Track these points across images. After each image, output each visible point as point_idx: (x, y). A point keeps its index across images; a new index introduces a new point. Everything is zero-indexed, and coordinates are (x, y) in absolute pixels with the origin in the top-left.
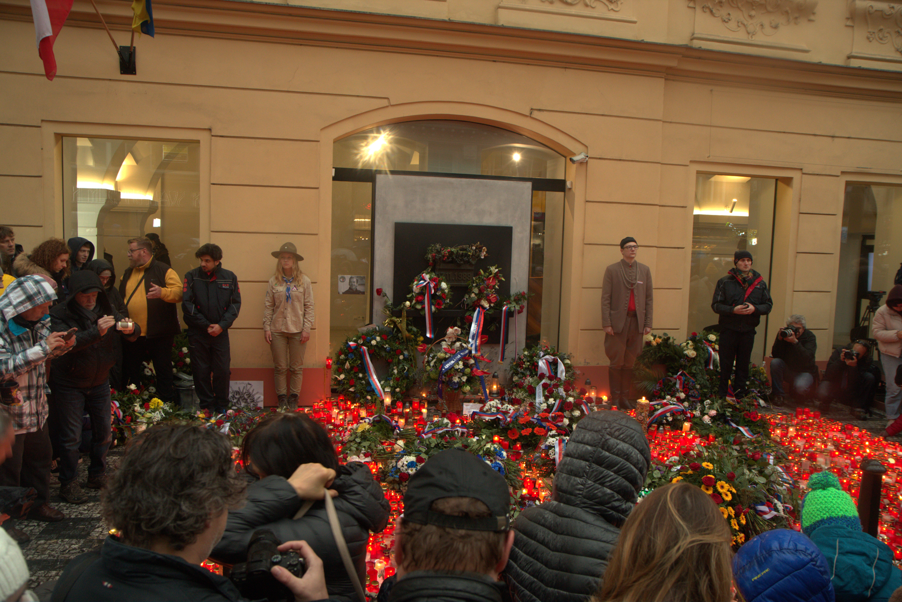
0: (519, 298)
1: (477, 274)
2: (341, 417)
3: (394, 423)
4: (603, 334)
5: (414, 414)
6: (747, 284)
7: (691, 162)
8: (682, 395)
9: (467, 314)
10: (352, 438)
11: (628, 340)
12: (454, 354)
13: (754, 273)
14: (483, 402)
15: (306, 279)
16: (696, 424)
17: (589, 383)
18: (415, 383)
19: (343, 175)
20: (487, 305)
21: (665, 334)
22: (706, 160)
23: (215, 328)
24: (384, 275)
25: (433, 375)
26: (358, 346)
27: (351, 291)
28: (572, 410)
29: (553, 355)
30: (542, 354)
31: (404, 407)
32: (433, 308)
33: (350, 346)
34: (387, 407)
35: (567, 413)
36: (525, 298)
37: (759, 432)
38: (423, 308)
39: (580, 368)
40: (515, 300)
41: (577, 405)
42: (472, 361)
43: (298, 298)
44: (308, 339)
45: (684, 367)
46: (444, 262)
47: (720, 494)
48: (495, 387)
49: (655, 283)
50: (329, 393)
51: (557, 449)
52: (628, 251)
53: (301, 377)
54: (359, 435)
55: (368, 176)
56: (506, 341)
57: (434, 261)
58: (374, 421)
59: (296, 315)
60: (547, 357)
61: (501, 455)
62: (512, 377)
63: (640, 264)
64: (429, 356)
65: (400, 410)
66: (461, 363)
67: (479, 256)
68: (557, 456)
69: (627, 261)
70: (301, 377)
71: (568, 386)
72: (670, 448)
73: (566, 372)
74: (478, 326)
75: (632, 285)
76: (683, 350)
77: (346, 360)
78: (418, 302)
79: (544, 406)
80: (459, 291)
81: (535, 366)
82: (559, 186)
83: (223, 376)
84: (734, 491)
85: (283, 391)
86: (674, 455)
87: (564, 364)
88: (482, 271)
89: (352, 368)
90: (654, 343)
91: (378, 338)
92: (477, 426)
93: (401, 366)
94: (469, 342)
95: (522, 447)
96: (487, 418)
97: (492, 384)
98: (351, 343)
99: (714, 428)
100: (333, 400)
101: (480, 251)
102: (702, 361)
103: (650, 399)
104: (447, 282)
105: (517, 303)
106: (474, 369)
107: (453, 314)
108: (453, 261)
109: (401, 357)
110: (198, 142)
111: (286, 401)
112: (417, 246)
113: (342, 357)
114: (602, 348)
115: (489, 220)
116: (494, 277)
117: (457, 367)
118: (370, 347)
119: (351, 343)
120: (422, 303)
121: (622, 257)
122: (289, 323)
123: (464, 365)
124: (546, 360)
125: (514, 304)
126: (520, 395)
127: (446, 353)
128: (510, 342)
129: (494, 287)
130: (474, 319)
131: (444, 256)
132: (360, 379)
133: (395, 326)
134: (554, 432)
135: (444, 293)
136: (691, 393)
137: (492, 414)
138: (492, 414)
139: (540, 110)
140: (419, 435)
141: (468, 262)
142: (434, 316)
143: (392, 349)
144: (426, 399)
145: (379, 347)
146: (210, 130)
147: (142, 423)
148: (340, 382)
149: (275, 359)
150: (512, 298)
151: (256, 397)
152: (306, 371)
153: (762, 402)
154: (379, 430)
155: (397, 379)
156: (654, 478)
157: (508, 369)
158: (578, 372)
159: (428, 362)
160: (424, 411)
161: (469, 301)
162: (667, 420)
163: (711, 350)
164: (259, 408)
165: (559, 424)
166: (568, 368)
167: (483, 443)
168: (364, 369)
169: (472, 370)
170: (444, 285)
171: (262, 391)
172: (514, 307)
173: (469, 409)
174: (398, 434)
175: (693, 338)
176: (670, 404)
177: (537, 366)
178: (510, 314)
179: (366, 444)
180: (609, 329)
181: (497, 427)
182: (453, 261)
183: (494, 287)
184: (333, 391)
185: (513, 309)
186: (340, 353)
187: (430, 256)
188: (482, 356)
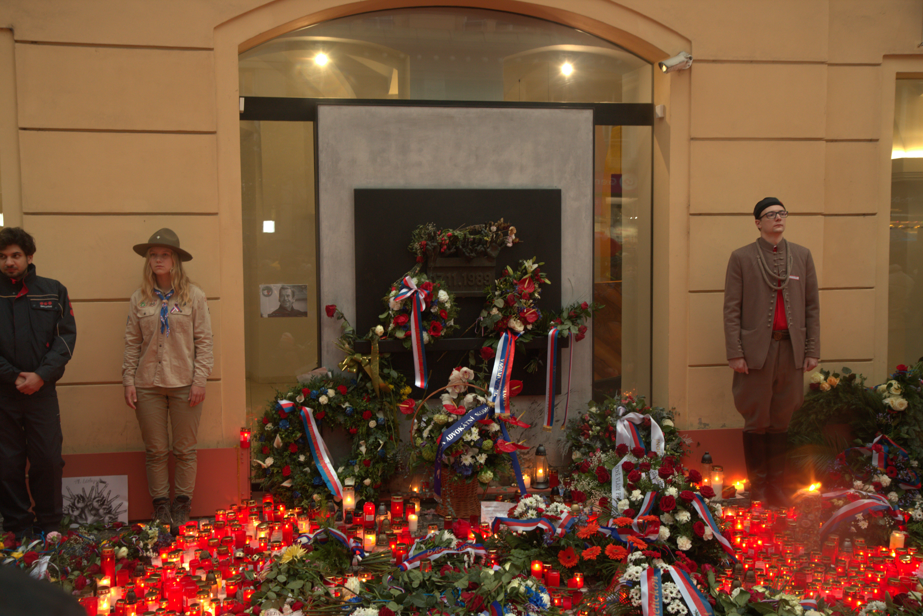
0: (577, 314)
1: (502, 274)
2: (262, 534)
3: (352, 543)
4: (728, 374)
5: (392, 524)
7: (886, 57)
9: (486, 344)
10: (272, 575)
11: (775, 383)
12: (464, 415)
14: (516, 499)
15: (197, 293)
16: (915, 534)
17: (709, 461)
18: (397, 468)
19: (257, 109)
20: (519, 328)
21: (846, 370)
23: (29, 380)
24: (340, 284)
25: (427, 454)
26: (296, 408)
27: (283, 312)
28: (676, 512)
29: (642, 411)
30: (621, 410)
31: (377, 512)
32: (426, 336)
33: (281, 407)
34: (348, 513)
35: (666, 517)
36: (587, 314)
38: (408, 336)
39: (691, 434)
41: (684, 502)
42: (495, 427)
43: (181, 325)
44: (202, 397)
45: (885, 429)
46: (442, 255)
48: (540, 472)
50: (246, 491)
51: (645, 588)
52: (769, 223)
53: (193, 465)
54: (283, 568)
55: (303, 110)
56: (557, 389)
57: (425, 252)
58: (316, 541)
60: (631, 415)
61: (538, 601)
62: (570, 453)
63: (792, 245)
64: (420, 421)
65: (369, 518)
66: (475, 431)
67: (503, 243)
68: (645, 602)
69: (769, 240)
70: (193, 465)
71: (668, 467)
72: (868, 582)
73: (667, 441)
74: (506, 364)
75: (780, 282)
76: (880, 397)
77: (276, 432)
78: (398, 326)
79: (624, 505)
80: (471, 304)
81: (611, 432)
82: (643, 115)
85: (162, 491)
86: (875, 598)
87: (663, 428)
89: (286, 446)
90: (826, 386)
91: (331, 392)
92: (503, 545)
93: (372, 440)
94: (489, 394)
95: (585, 580)
96: (521, 529)
97: (535, 467)
98: (284, 402)
100: (253, 503)
101: (506, 234)
104: (449, 290)
105: (573, 323)
106: (500, 441)
107: (462, 345)
108: (458, 254)
109: (372, 424)
111: (167, 509)
112: (390, 225)
113: (270, 426)
114: (730, 398)
115: (518, 180)
116: (531, 278)
117: (468, 438)
118: (317, 407)
119: (284, 402)
121: (758, 234)
122: (167, 370)
123: (480, 434)
124: (631, 421)
125: (568, 324)
126: (584, 484)
127: (449, 415)
128: (564, 390)
129: (531, 296)
131: (441, 245)
132: (301, 464)
133: (360, 369)
134: (638, 555)
137: (530, 522)
138: (530, 522)
140: (399, 563)
141: (485, 254)
142: (428, 351)
143: (354, 411)
144: (417, 497)
145: (335, 407)
146: (11, 30)
148: (265, 472)
149: (146, 435)
150: (565, 315)
151: (114, 504)
152: (203, 455)
154: (326, 556)
155: (366, 463)
157: (563, 438)
158: (688, 441)
159: (420, 431)
160: (413, 518)
161: (488, 322)
162: (858, 528)
164: (121, 524)
165: (652, 537)
166: (670, 434)
167: (504, 580)
168: (306, 445)
169: (495, 442)
170: (443, 295)
171: (125, 493)
172: (568, 329)
173: (490, 512)
174: (359, 563)
175: (901, 375)
178: (562, 342)
179: (296, 585)
180: (741, 364)
181: (539, 545)
182: (458, 254)
183: (531, 296)
184: (255, 488)
185: (566, 333)
186: (265, 421)
187: (417, 245)
188: (513, 417)
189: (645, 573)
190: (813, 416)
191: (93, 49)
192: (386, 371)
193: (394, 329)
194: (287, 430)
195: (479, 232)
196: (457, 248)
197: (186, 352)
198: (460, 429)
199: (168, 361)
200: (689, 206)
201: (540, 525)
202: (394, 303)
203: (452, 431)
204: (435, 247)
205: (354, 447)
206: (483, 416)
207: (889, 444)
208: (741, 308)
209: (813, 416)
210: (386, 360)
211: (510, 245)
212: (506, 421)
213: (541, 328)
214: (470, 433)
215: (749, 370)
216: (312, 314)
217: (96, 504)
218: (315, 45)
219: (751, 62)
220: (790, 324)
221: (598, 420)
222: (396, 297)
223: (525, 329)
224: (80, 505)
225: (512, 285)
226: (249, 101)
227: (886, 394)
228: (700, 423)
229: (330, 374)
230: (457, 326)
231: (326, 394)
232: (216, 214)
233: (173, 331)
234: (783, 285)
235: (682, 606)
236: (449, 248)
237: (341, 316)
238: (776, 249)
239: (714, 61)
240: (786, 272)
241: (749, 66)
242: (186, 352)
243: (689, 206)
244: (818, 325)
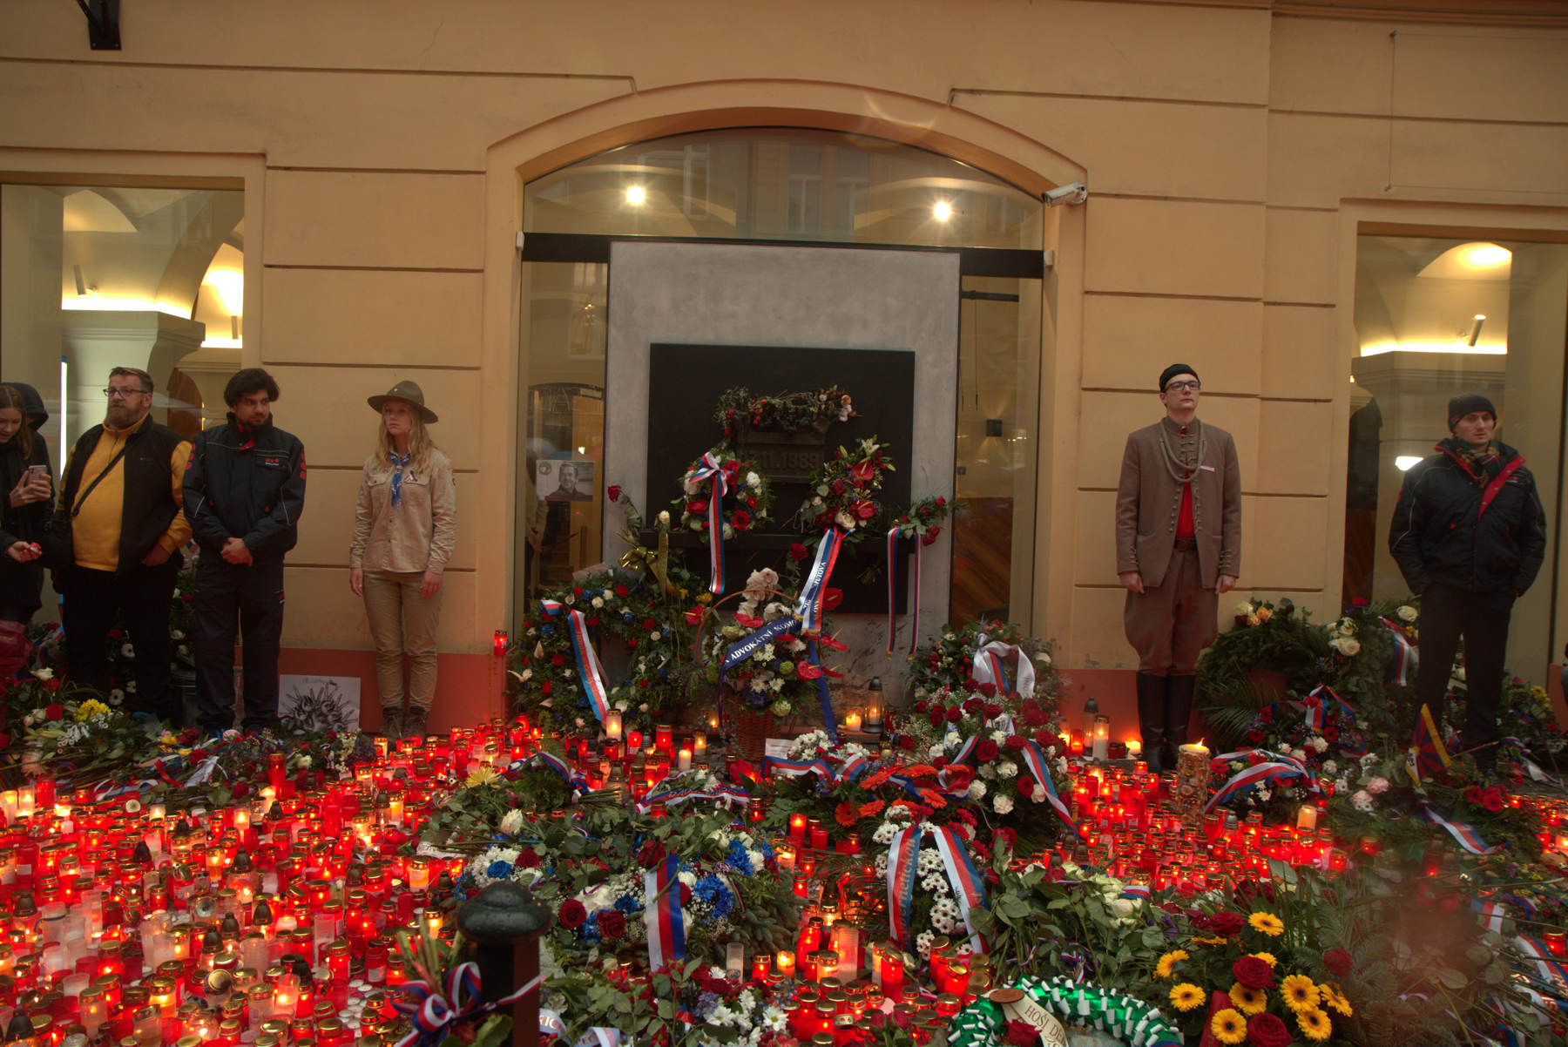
0: (930, 511)
1: (833, 456)
6: (1485, 476)
7: (1344, 201)
8: (1321, 744)
9: (807, 543)
11: (1178, 607)
12: (760, 629)
13: (1503, 449)
15: (438, 459)
16: (1333, 810)
17: (1094, 709)
19: (542, 248)
20: (849, 523)
22: (1383, 195)
24: (628, 460)
26: (564, 610)
28: (999, 763)
29: (1008, 642)
37: (1503, 842)
38: (706, 528)
39: (1073, 673)
40: (919, 515)
42: (800, 646)
43: (415, 496)
45: (1329, 679)
47: (1293, 1015)
49: (1248, 477)
51: (894, 854)
52: (1176, 396)
55: (595, 249)
56: (901, 609)
57: (732, 424)
59: (413, 535)
60: (994, 645)
62: (913, 687)
66: (770, 648)
67: (837, 416)
68: (891, 872)
69: (1177, 419)
73: (1038, 680)
75: (1188, 473)
77: (538, 638)
78: (695, 515)
80: (788, 493)
81: (966, 665)
83: (265, 665)
84: (1345, 1008)
85: (393, 699)
87: (1035, 663)
88: (843, 450)
89: (548, 656)
90: (1255, 620)
91: (608, 594)
93: (652, 655)
94: (798, 605)
99: (1381, 824)
101: (839, 406)
102: (1377, 665)
103: (1215, 746)
105: (923, 523)
108: (774, 427)
109: (655, 636)
110: (242, 180)
112: (695, 390)
116: (870, 463)
117: (759, 656)
120: (704, 518)
122: (397, 551)
124: (992, 652)
129: (866, 484)
130: (820, 555)
131: (753, 415)
133: (647, 568)
135: (752, 496)
136: (1343, 738)
139: (972, 92)
141: (809, 429)
142: (727, 547)
145: (611, 612)
146: (263, 155)
147: (33, 748)
150: (913, 511)
151: (345, 711)
153: (1534, 771)
155: (644, 684)
156: (1141, 948)
157: (907, 670)
158: (1067, 682)
159: (710, 647)
162: (1257, 799)
163: (1402, 640)
165: (959, 794)
166: (1042, 672)
168: (573, 658)
170: (753, 478)
171: (357, 698)
176: (1286, 760)
177: (971, 665)
178: (906, 546)
180: (1134, 579)
182: (774, 427)
185: (909, 533)
187: (722, 415)
189: (901, 834)
190: (1234, 658)
191: (350, 175)
192: (675, 570)
193: (689, 519)
194: (550, 637)
195: (805, 402)
196: (774, 420)
197: (421, 530)
198: (752, 645)
199: (399, 541)
200: (1080, 379)
201: (813, 769)
202: (689, 483)
203: (741, 647)
204: (744, 418)
205: (632, 663)
206: (783, 631)
207: (1330, 697)
208: (1138, 507)
209: (1234, 658)
210: (679, 557)
211: (844, 419)
212: (814, 638)
213: (878, 526)
214: (763, 650)
215: (1145, 588)
216: (597, 499)
217: (324, 709)
218: (631, 176)
219: (1166, 198)
220: (1198, 528)
221: (951, 649)
222: (692, 478)
223: (857, 526)
224: (307, 709)
225: (845, 470)
226: (529, 237)
227: (1335, 634)
228: (1088, 661)
229: (611, 573)
230: (771, 519)
231: (601, 595)
232: (478, 369)
233: (404, 504)
234: (1192, 476)
235: (942, 881)
236: (764, 419)
237: (627, 500)
238: (1184, 431)
239: (1117, 196)
240: (1196, 461)
241: (1162, 203)
242: (421, 530)
243: (1080, 379)
244: (1238, 533)
